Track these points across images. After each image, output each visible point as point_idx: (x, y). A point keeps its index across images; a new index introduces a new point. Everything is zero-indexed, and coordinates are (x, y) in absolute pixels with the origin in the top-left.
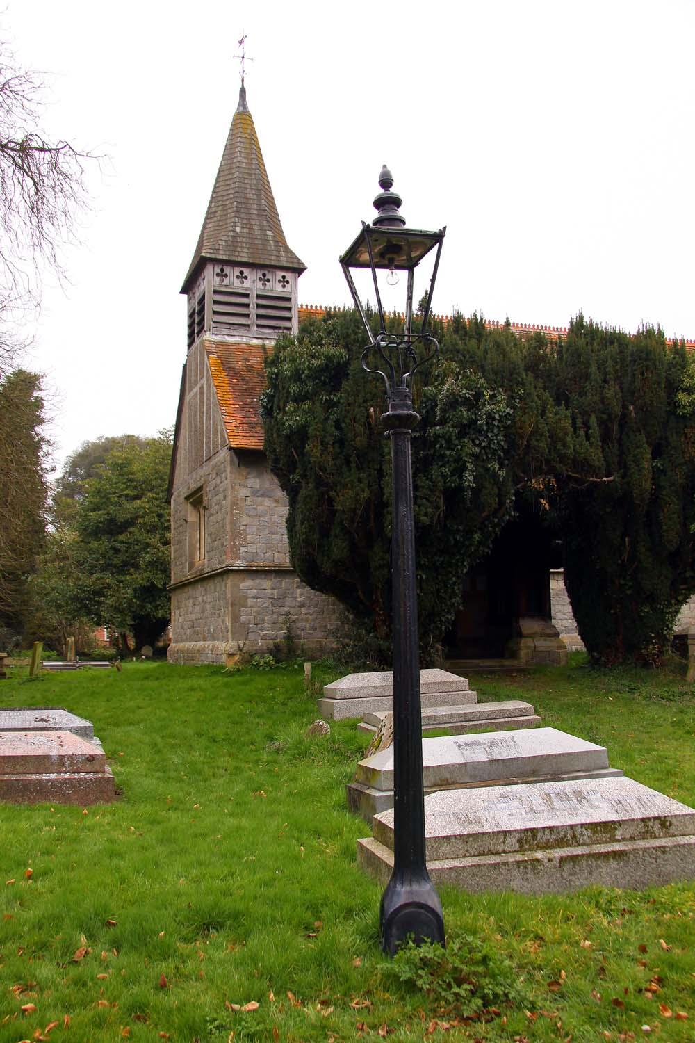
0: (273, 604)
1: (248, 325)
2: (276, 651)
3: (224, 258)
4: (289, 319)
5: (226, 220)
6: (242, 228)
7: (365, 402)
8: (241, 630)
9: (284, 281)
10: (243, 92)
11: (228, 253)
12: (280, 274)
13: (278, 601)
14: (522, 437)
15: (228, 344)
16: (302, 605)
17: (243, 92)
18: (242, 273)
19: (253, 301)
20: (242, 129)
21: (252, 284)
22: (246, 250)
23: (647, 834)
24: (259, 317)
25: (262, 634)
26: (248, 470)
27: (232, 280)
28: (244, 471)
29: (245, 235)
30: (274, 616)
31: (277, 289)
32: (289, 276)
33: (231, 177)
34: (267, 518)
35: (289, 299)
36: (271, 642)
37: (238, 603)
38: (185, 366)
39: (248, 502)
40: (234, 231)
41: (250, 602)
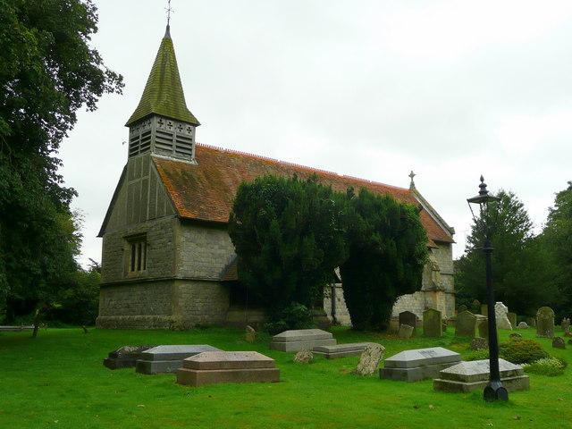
4: (191, 150)
9: (189, 130)
10: (168, 28)
12: (188, 126)
15: (162, 159)
17: (168, 28)
19: (175, 138)
20: (167, 44)
21: (174, 129)
27: (165, 127)
31: (185, 133)
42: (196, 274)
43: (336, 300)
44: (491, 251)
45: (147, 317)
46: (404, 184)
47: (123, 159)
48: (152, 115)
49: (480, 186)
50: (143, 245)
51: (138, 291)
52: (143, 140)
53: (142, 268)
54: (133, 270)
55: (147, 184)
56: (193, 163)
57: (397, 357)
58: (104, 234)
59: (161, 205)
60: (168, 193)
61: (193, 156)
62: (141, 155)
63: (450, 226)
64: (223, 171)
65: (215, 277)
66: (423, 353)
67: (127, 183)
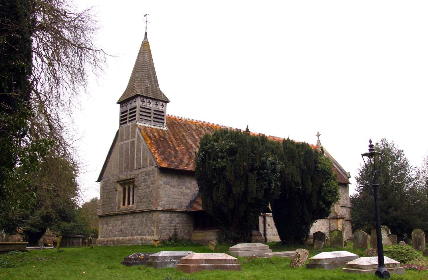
0: (169, 223)
1: (151, 121)
2: (170, 239)
3: (145, 95)
5: (143, 81)
6: (149, 85)
7: (243, 161)
8: (160, 232)
9: (162, 106)
10: (146, 34)
11: (146, 93)
12: (161, 103)
13: (171, 222)
14: (285, 175)
16: (178, 224)
17: (146, 34)
18: (149, 101)
20: (145, 46)
21: (152, 105)
22: (151, 93)
23: (394, 266)
24: (154, 118)
25: (166, 233)
26: (162, 175)
27: (146, 104)
28: (161, 175)
29: (150, 87)
30: (170, 227)
31: (160, 108)
32: (164, 104)
33: (144, 65)
34: (168, 192)
35: (163, 112)
36: (169, 236)
37: (159, 222)
38: (118, 133)
39: (162, 186)
40: (147, 85)
41: (162, 222)
42: (171, 207)
43: (267, 225)
44: (378, 186)
45: (135, 237)
46: (244, 128)
47: (115, 126)
48: (137, 96)
49: (369, 146)
50: (131, 186)
51: (129, 219)
52: (130, 114)
53: (131, 203)
54: (124, 204)
55: (134, 144)
56: (165, 128)
57: (317, 257)
58: (101, 179)
59: (145, 159)
60: (150, 150)
61: (165, 124)
62: (129, 124)
63: (347, 172)
64: (186, 134)
65: (183, 209)
66: (334, 254)
67: (118, 143)
